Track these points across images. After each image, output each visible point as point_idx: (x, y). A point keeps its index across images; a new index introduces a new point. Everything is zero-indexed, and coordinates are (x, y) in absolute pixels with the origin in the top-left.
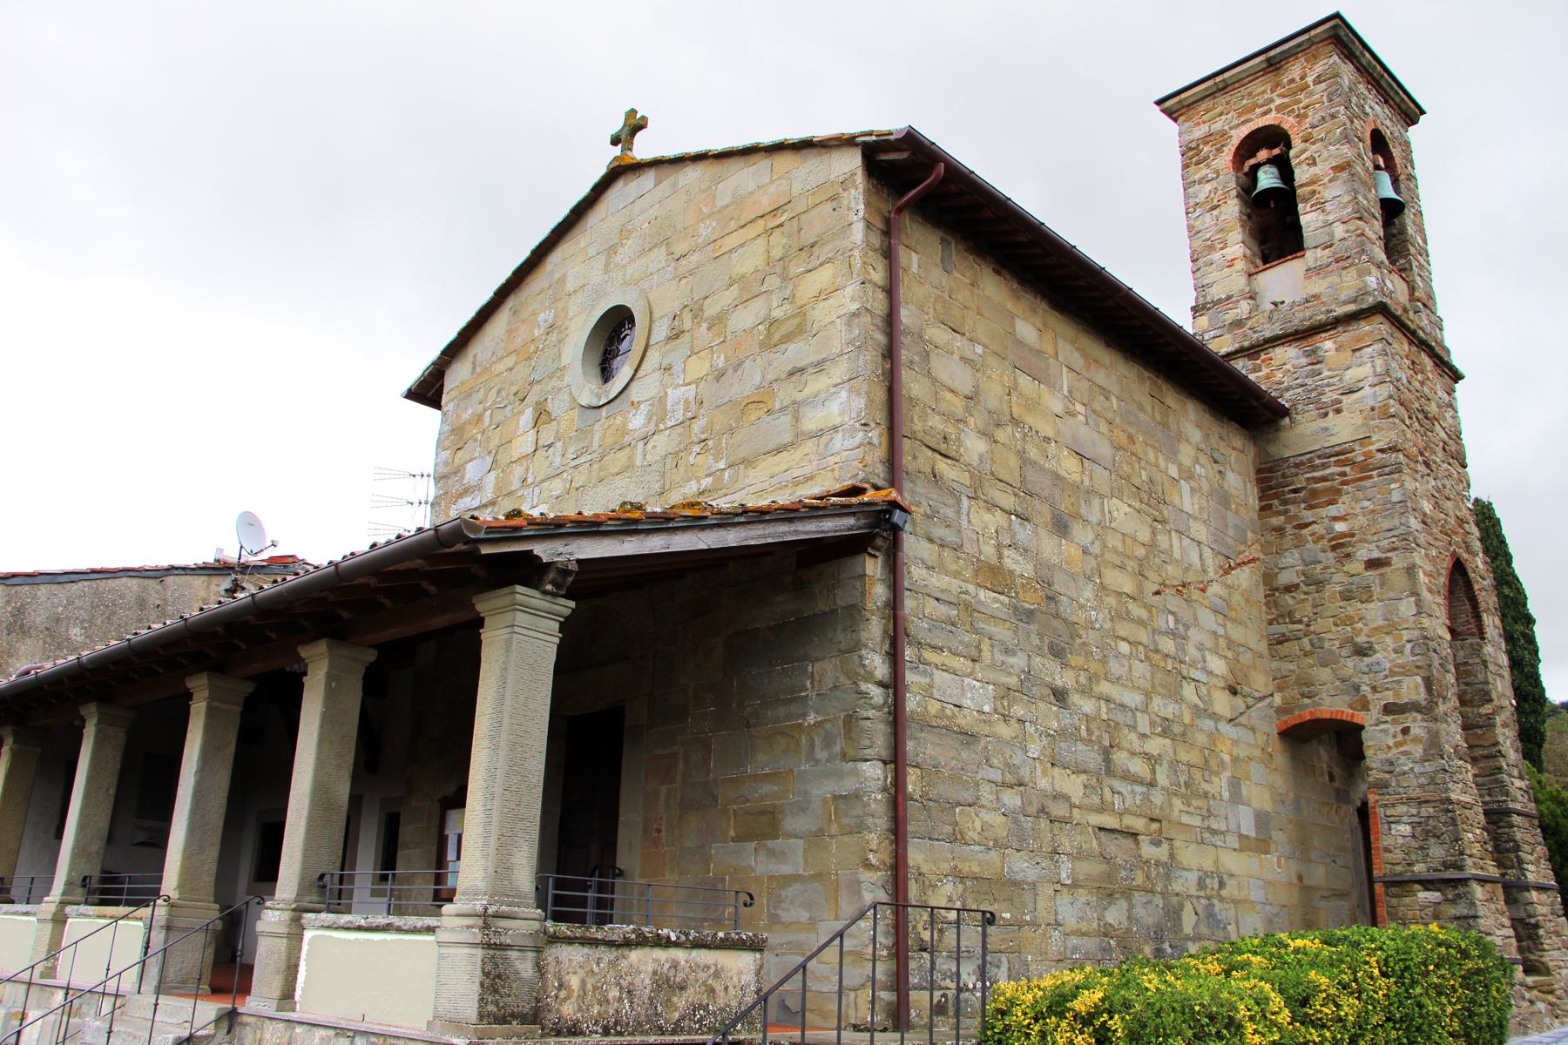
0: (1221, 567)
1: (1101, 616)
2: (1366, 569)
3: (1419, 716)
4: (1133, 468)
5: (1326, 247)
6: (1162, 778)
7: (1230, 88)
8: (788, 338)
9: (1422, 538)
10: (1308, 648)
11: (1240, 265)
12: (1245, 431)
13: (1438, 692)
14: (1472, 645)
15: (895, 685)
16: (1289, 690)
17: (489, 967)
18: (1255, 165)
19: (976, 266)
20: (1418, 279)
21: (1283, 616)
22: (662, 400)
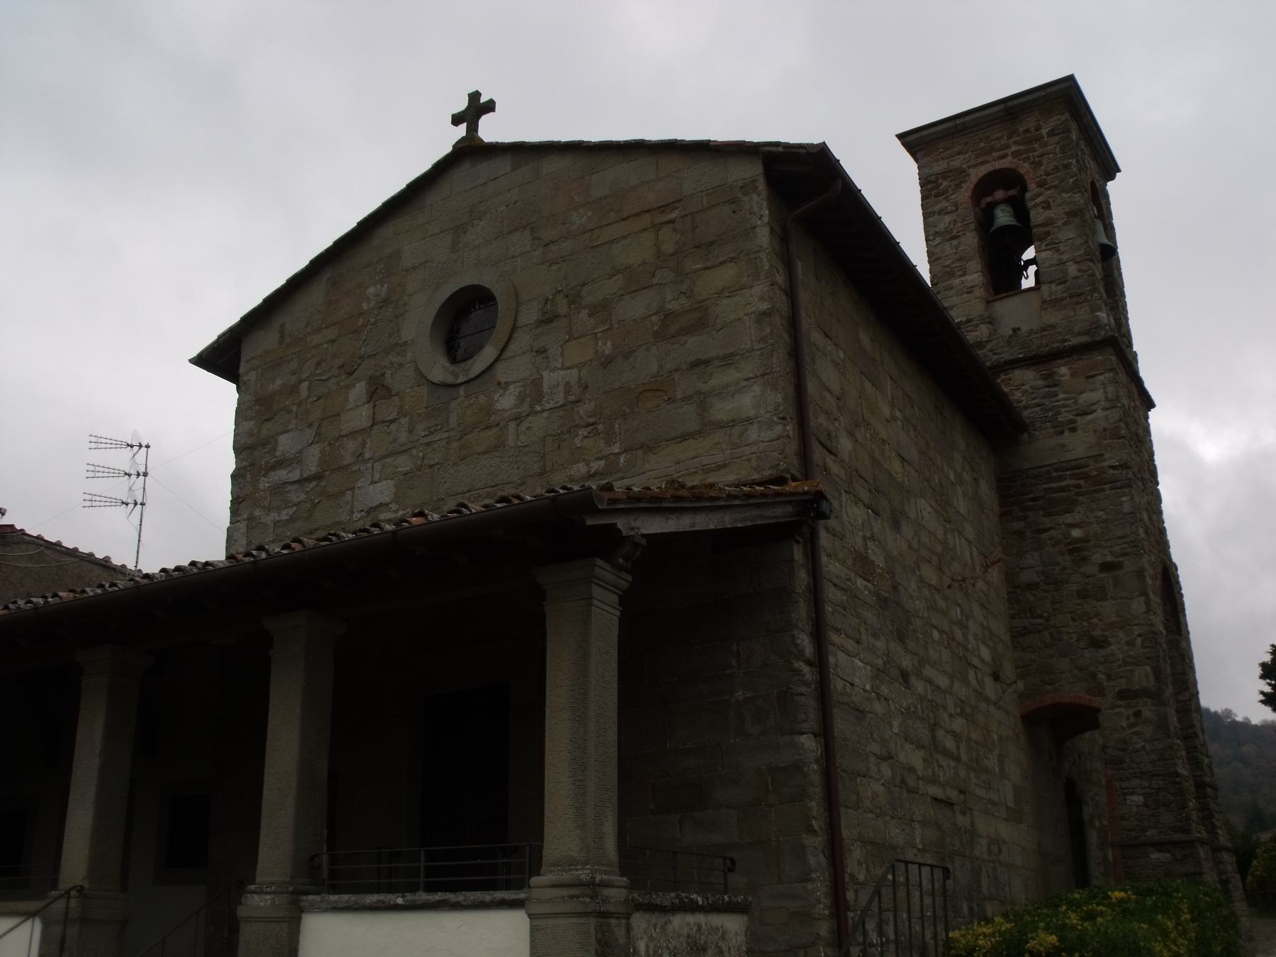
3: (1149, 701)
8: (688, 330)
11: (979, 292)
15: (820, 663)
17: (599, 935)
18: (991, 202)
22: (537, 383)
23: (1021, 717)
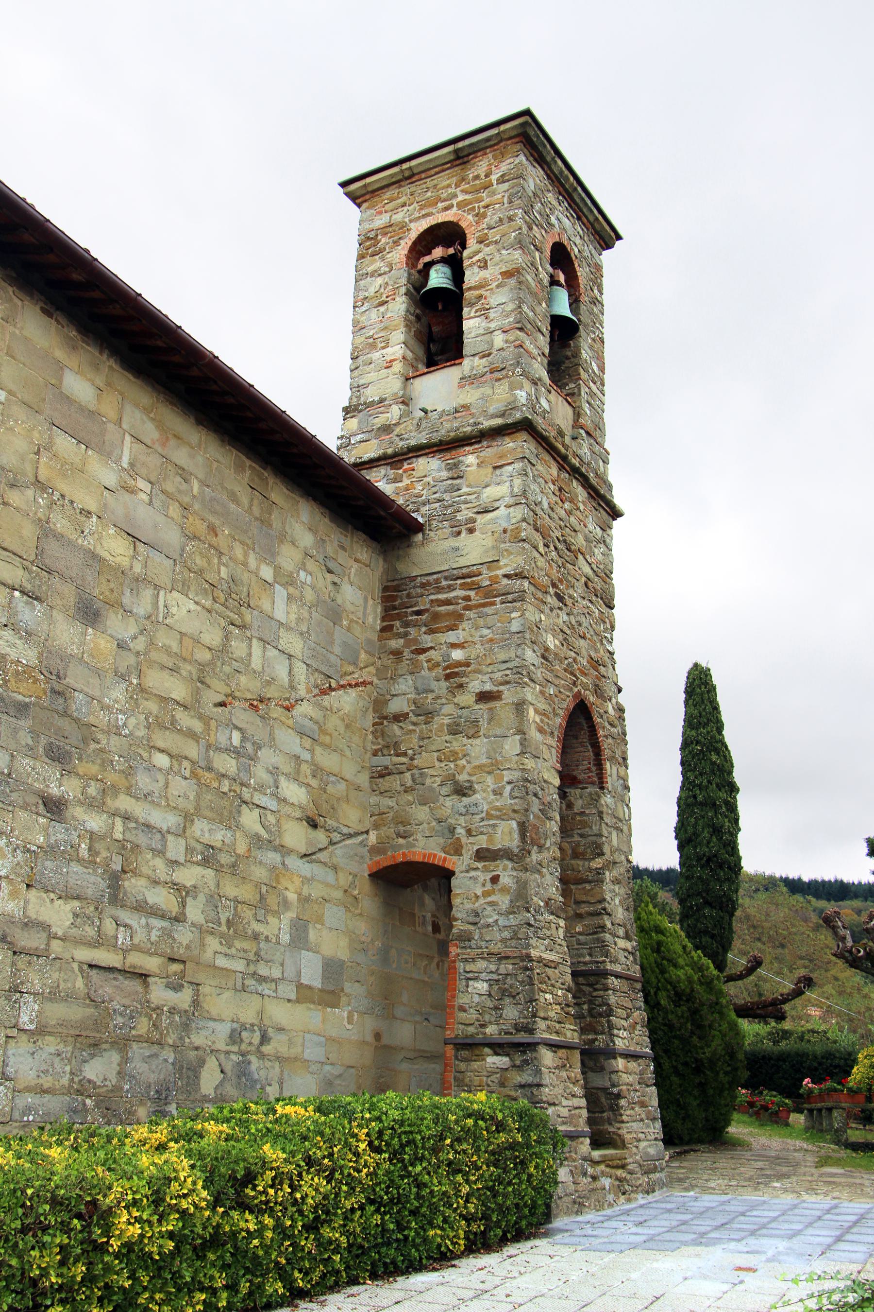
0: (317, 686)
1: (132, 721)
2: (477, 701)
3: (510, 864)
4: (209, 562)
5: (484, 357)
6: (195, 911)
7: (416, 177)
9: (539, 675)
10: (409, 783)
11: (398, 367)
12: (375, 544)
13: (532, 839)
14: (590, 794)
16: (385, 828)
19: (16, 300)
20: (586, 407)
21: (388, 747)
23: (369, 875)
